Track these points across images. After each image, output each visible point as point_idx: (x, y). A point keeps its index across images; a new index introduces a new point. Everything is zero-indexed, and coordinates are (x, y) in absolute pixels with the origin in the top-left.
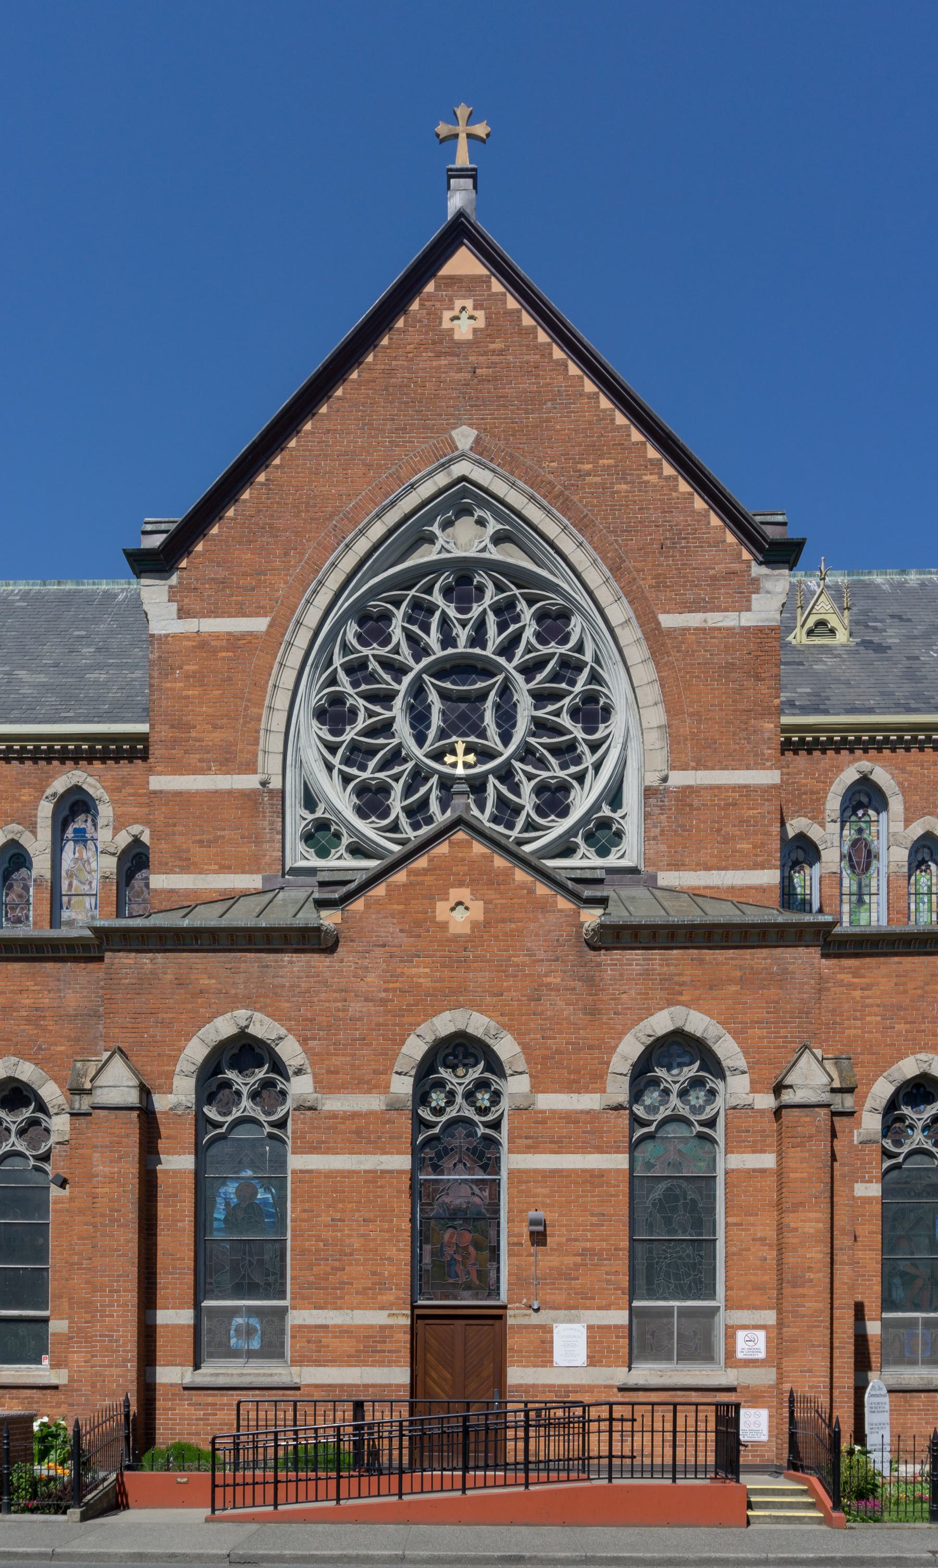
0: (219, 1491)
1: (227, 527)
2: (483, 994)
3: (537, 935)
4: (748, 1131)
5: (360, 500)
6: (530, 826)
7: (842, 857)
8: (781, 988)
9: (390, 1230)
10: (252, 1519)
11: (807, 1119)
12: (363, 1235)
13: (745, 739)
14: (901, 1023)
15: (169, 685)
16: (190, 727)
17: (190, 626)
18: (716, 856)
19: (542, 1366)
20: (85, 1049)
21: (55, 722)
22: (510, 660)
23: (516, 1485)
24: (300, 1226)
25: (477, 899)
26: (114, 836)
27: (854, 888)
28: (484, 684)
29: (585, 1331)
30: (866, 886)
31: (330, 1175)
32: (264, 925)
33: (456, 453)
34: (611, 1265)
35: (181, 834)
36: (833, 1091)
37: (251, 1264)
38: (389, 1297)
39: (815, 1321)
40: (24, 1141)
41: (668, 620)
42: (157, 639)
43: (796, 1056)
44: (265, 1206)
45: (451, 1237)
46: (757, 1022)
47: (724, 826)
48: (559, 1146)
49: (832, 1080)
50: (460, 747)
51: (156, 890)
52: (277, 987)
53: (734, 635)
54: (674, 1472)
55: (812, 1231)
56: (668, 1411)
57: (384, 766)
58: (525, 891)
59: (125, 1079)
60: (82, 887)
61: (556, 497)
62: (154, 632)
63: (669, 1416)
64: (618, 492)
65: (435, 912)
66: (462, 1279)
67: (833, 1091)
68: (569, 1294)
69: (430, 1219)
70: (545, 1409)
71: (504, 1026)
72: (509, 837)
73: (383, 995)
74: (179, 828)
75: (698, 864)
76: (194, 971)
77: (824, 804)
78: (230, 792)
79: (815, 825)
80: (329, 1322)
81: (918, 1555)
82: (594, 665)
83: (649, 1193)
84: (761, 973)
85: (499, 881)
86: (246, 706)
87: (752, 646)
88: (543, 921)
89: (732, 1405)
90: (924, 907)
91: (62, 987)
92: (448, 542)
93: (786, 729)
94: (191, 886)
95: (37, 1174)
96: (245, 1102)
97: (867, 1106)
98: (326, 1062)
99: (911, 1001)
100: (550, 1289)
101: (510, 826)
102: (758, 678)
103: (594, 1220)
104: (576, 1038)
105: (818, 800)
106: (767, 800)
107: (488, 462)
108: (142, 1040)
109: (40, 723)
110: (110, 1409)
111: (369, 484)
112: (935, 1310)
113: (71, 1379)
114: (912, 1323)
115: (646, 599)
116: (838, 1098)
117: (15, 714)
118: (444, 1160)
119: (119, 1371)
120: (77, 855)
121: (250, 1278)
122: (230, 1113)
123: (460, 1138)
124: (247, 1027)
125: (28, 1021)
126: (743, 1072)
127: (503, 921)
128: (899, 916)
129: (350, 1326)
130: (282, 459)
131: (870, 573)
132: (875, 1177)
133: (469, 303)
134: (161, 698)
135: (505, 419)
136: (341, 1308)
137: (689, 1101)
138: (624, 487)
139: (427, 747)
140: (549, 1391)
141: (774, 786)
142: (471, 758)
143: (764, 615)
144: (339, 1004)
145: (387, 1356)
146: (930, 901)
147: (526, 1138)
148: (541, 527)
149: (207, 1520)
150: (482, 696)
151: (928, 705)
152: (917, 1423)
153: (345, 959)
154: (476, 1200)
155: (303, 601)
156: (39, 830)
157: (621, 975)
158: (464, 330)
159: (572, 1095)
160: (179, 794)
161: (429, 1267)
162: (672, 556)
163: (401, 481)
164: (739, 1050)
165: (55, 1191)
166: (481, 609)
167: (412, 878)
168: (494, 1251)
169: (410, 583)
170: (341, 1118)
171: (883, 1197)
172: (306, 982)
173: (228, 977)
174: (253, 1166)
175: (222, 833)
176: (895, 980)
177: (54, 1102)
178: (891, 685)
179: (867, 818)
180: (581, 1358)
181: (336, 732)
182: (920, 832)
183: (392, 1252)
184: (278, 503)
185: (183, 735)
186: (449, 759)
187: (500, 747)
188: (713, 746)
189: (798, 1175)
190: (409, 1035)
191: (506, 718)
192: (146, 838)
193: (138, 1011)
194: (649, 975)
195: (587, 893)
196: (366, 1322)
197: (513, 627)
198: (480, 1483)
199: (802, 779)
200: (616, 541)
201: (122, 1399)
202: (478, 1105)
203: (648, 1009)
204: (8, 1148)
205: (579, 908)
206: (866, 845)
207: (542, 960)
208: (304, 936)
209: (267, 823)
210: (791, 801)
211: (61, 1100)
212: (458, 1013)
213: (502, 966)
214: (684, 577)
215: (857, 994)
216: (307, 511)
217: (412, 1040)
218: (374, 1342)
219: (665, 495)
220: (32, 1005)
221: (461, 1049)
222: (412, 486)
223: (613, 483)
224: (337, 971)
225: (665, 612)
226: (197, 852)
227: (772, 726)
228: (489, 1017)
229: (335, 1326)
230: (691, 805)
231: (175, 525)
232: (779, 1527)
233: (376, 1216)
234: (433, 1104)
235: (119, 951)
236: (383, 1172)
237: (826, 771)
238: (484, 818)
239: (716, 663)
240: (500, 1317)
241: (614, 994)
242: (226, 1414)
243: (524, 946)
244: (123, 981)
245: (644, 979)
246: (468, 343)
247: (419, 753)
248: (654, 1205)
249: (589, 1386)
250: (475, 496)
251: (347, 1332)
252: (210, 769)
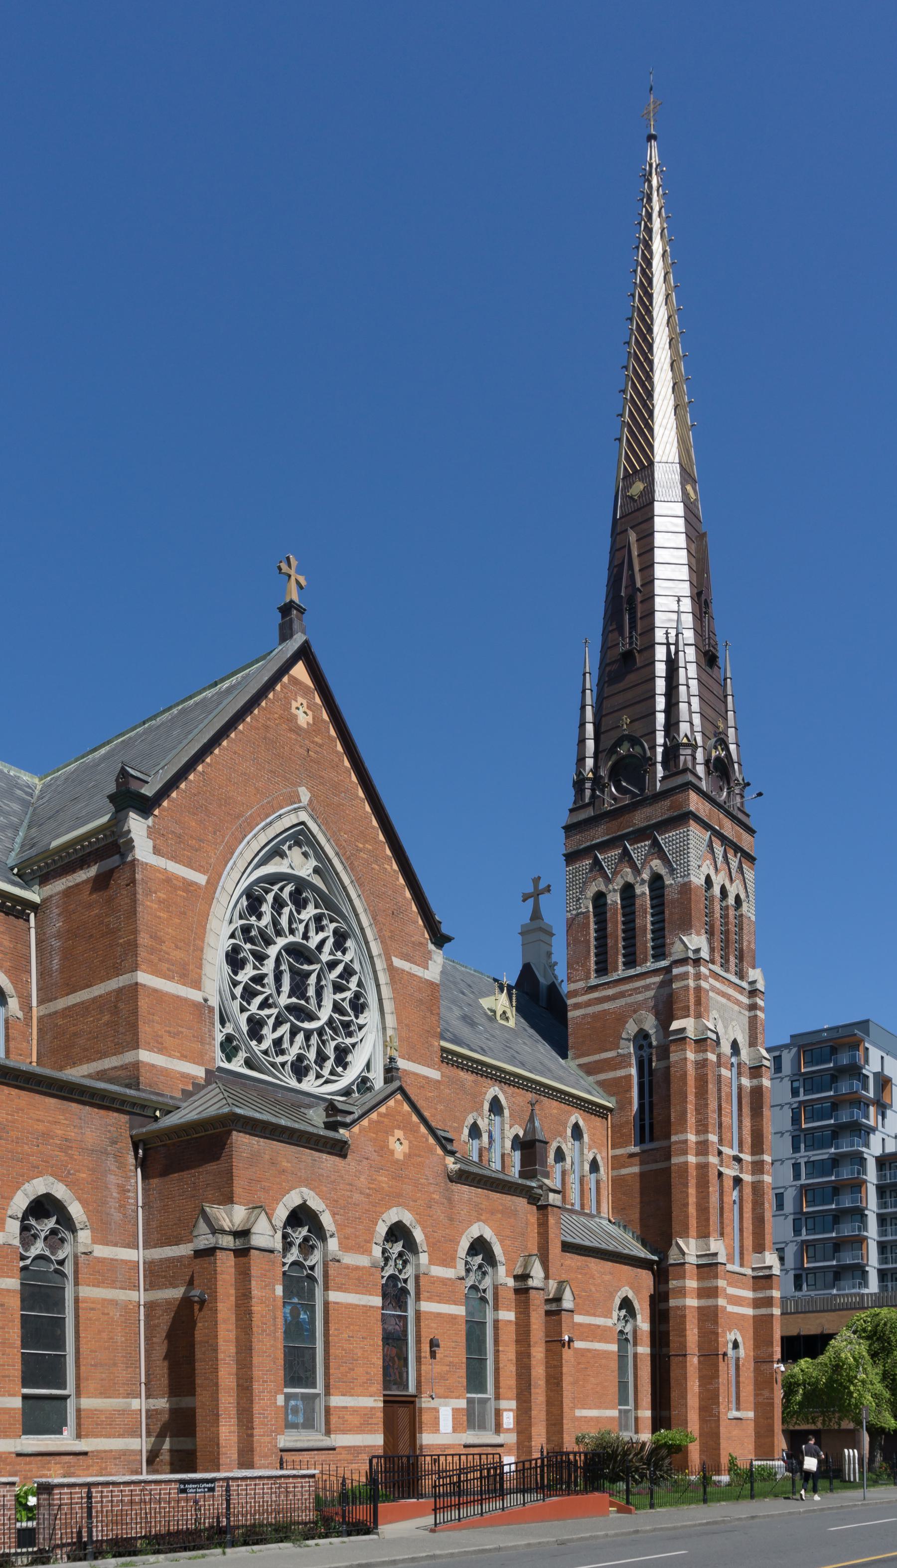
15: (149, 903)
57: (262, 1006)
73: (368, 1191)
74: (156, 1018)
85: (413, 1130)
95: (56, 1276)
103: (453, 1344)
150: (309, 974)
154: (397, 1327)
180: (450, 1429)
183: (374, 1360)
225: (396, 956)
226: (168, 1041)
229: (351, 1407)
235: (240, 1132)
240: (413, 1402)
250: (307, 837)
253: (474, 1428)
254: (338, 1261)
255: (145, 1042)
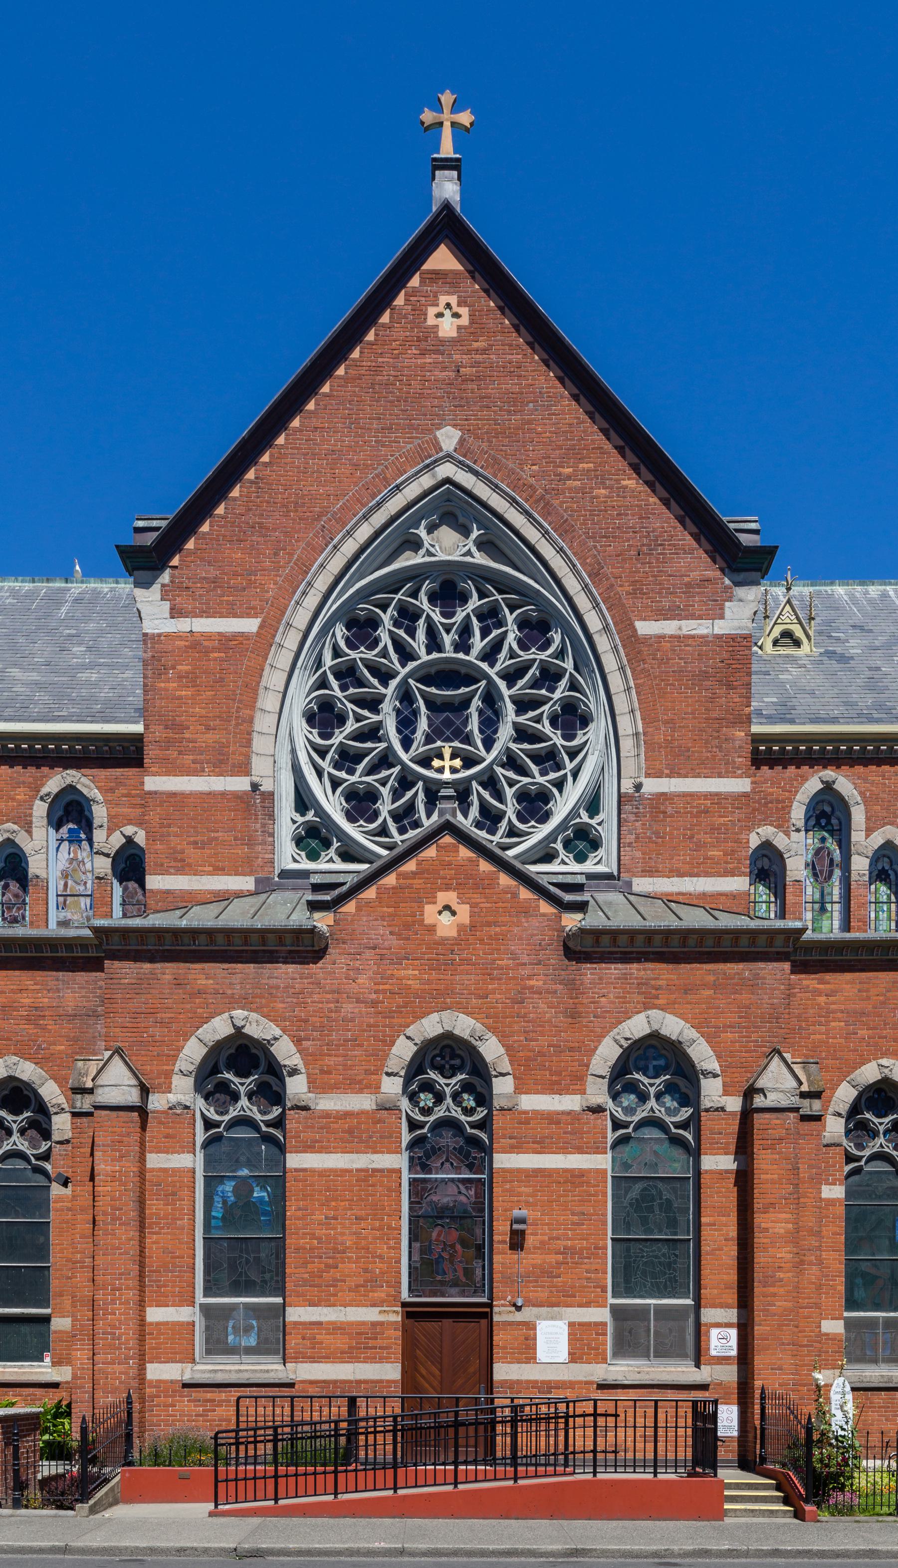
0: (222, 1486)
1: (217, 526)
2: (469, 996)
3: (520, 939)
4: (720, 1133)
5: (347, 500)
6: (512, 832)
7: (807, 865)
8: (753, 994)
9: (380, 1229)
10: (254, 1513)
11: (778, 1122)
12: (355, 1233)
13: (717, 747)
14: (863, 1029)
15: (163, 685)
16: (183, 728)
17: (184, 625)
18: (688, 863)
19: (526, 1363)
20: (84, 1049)
21: (48, 721)
22: (492, 665)
23: (505, 1479)
24: (295, 1224)
25: (463, 903)
26: (108, 837)
27: (817, 896)
28: (467, 690)
29: (566, 1328)
30: (829, 894)
31: (324, 1173)
32: (259, 927)
33: (441, 454)
34: (591, 1263)
35: (176, 836)
36: (803, 1095)
37: (247, 1261)
38: (380, 1294)
39: (785, 1320)
40: (25, 1140)
41: (644, 628)
42: (150, 639)
43: (766, 1061)
44: (261, 1204)
45: (439, 1235)
46: (729, 1027)
47: (697, 833)
48: (542, 1146)
49: (800, 1083)
50: (447, 753)
51: (152, 891)
52: (272, 987)
53: (707, 643)
54: (655, 1467)
55: (782, 1231)
56: (630, 1407)
58: (509, 895)
59: (126, 1078)
60: (78, 887)
61: (537, 501)
62: (147, 631)
63: (651, 1411)
64: (597, 497)
65: (423, 915)
66: (449, 1277)
67: (803, 1095)
68: (551, 1292)
69: (419, 1217)
70: (531, 1405)
71: (489, 1028)
72: (492, 842)
73: (374, 996)
75: (671, 871)
76: (192, 971)
77: (789, 813)
78: (223, 794)
79: (781, 834)
80: (323, 1319)
81: (890, 1548)
82: (573, 672)
83: (626, 1193)
84: (733, 978)
85: (484, 885)
86: (238, 707)
87: (725, 655)
88: (526, 924)
89: (709, 1401)
90: (883, 916)
91: (61, 986)
92: (433, 546)
93: (757, 739)
94: (186, 887)
96: (244, 1102)
97: (831, 1110)
98: (320, 1062)
99: (873, 1007)
100: (533, 1287)
101: (492, 832)
102: (730, 686)
104: (557, 1041)
105: (783, 808)
106: (738, 808)
107: (472, 464)
108: (141, 1039)
109: (34, 721)
110: (114, 1405)
111: (356, 485)
112: (895, 1310)
113: (75, 1376)
114: (873, 1322)
115: (623, 605)
116: (806, 1102)
117: (8, 712)
118: (433, 1158)
119: (122, 1368)
120: (72, 855)
121: (247, 1275)
122: (227, 1112)
123: (447, 1138)
124: (243, 1027)
125: (28, 1020)
126: (715, 1076)
127: (489, 924)
128: (860, 924)
129: (342, 1323)
130: (271, 456)
131: (832, 584)
132: (839, 1180)
133: (453, 300)
134: (154, 699)
135: (487, 420)
136: (334, 1305)
137: (664, 1103)
138: (603, 491)
139: (412, 752)
140: (533, 1387)
141: (745, 795)
142: (457, 763)
143: (736, 623)
144: (332, 1005)
145: (378, 1353)
146: (889, 910)
147: (510, 1138)
148: (523, 531)
149: (211, 1514)
150: (466, 703)
151: (889, 716)
152: (878, 1420)
153: (338, 961)
154: (463, 1199)
155: (293, 602)
156: (34, 830)
157: (601, 979)
158: (447, 327)
159: (553, 1096)
160: (174, 794)
161: (418, 1265)
162: (649, 563)
163: (387, 482)
164: (712, 1053)
165: (56, 1190)
166: (464, 614)
167: (401, 881)
168: (480, 1250)
169: (397, 586)
170: (334, 1118)
171: (847, 1199)
172: (300, 983)
173: (225, 978)
174: (250, 1164)
175: (216, 835)
176: (858, 986)
177: (54, 1102)
178: (854, 696)
179: (830, 828)
180: (563, 1354)
181: (325, 736)
182: (881, 841)
184: (268, 502)
185: (177, 736)
186: (436, 763)
187: (483, 753)
188: (686, 754)
189: (769, 1176)
190: (398, 1036)
191: (490, 725)
192: (140, 838)
193: (138, 1010)
194: (626, 979)
195: (568, 897)
196: (359, 1319)
197: (495, 633)
198: (471, 1477)
199: (767, 787)
200: (595, 547)
201: (125, 1395)
202: (464, 1105)
203: (626, 1012)
204: (9, 1147)
205: (560, 913)
206: (829, 854)
207: (525, 964)
208: (298, 938)
209: (259, 825)
210: (758, 810)
211: (62, 1100)
212: (446, 1014)
213: (487, 969)
214: (660, 584)
215: (822, 999)
216: (296, 511)
217: (401, 1041)
218: (365, 1338)
219: (642, 500)
220: (33, 1005)
221: (448, 1050)
222: (398, 488)
223: (592, 488)
224: (330, 973)
226: (192, 854)
227: (743, 734)
228: (475, 1019)
230: (664, 812)
231: (167, 522)
232: (755, 1520)
233: (368, 1215)
234: (422, 1104)
236: (375, 1170)
237: (791, 780)
238: (466, 822)
239: (690, 672)
241: (594, 998)
242: (224, 1411)
243: (508, 949)
244: (123, 981)
245: (622, 983)
246: (453, 341)
247: (404, 756)
248: (631, 1204)
249: (571, 1382)
251: (340, 1328)
252: (204, 771)
253: (648, 1356)
254: (306, 1108)
255: (156, 864)
